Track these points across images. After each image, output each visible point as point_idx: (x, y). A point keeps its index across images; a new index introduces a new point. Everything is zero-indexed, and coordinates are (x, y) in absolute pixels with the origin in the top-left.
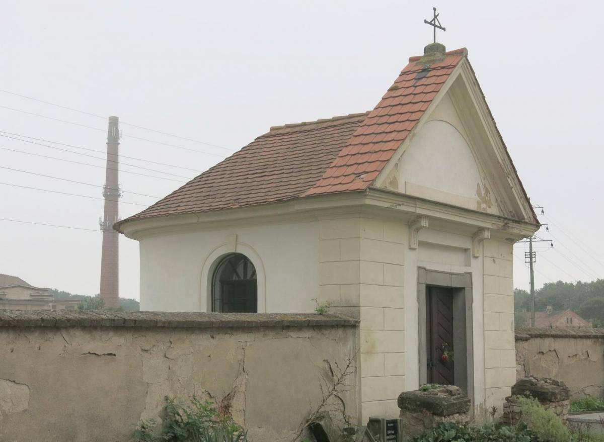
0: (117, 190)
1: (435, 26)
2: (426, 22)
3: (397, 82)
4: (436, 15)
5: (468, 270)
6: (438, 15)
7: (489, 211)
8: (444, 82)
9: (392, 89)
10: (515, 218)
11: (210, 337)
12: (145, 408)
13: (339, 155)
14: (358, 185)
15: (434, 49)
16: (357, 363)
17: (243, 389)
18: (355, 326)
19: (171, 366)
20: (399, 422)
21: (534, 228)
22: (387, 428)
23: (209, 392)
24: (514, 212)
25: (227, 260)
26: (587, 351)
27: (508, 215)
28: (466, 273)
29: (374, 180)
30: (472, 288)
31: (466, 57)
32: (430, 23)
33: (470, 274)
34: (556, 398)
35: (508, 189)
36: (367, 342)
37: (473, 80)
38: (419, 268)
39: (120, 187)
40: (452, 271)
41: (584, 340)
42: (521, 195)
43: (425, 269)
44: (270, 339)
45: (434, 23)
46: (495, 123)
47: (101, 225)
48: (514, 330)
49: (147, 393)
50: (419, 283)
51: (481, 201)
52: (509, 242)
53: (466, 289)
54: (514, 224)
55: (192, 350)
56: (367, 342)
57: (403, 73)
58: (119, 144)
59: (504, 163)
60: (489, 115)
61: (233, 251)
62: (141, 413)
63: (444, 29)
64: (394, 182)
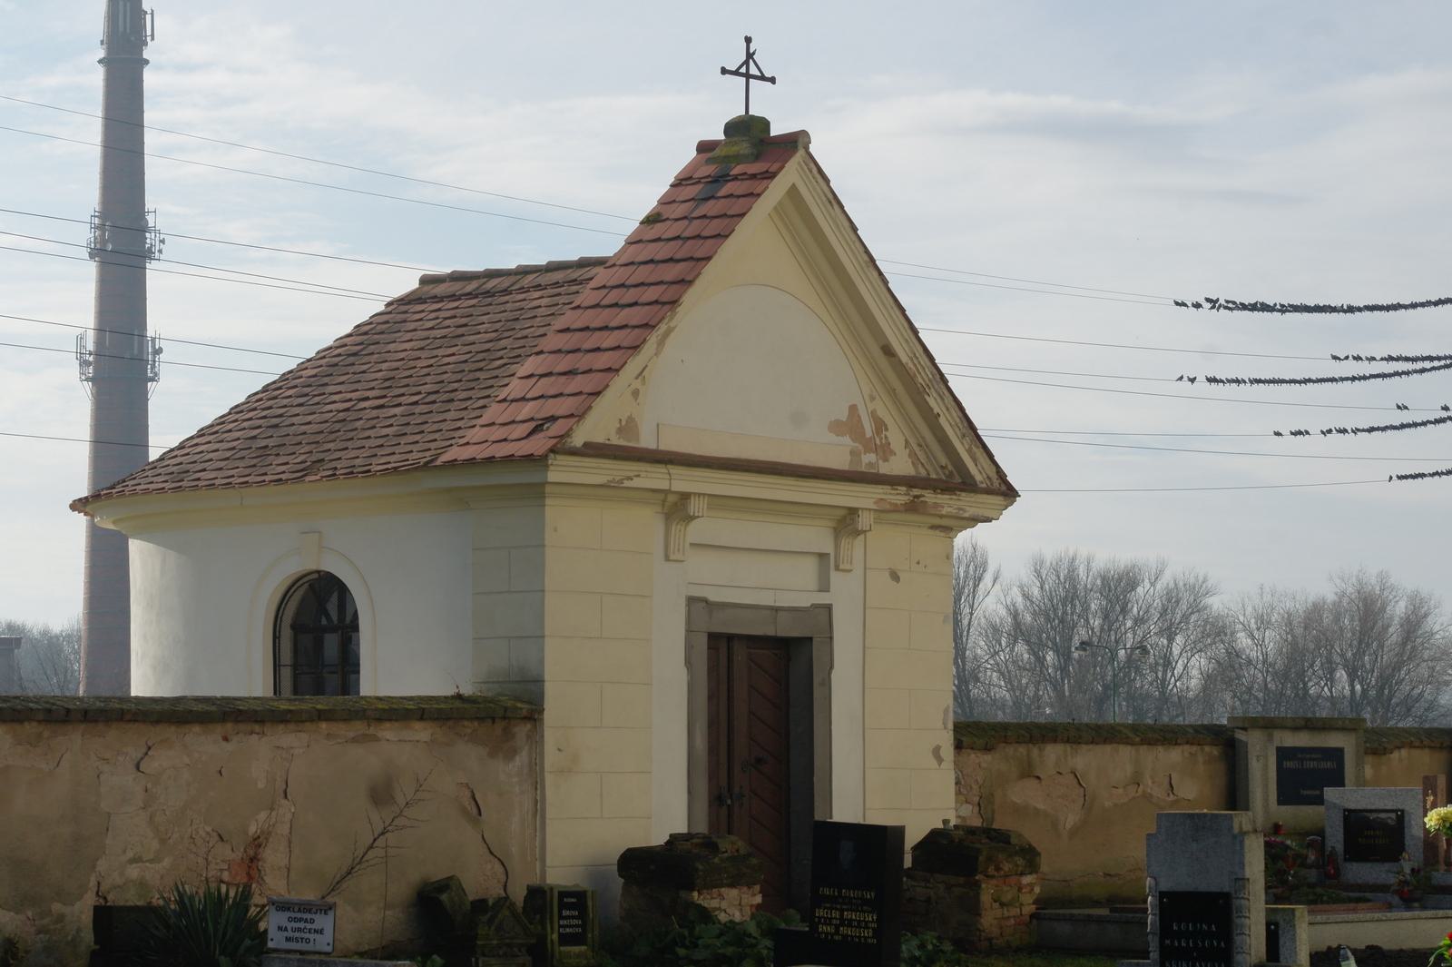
0: (142, 229)
1: (748, 76)
2: (724, 71)
3: (665, 204)
4: (751, 51)
5: (823, 599)
6: (754, 53)
7: (885, 469)
8: (743, 215)
9: (651, 220)
10: (960, 477)
11: (220, 738)
12: (104, 853)
13: (518, 375)
14: (538, 445)
15: (748, 129)
16: (538, 792)
17: (285, 829)
18: (534, 715)
19: (149, 786)
20: (589, 894)
21: (998, 500)
22: (559, 904)
23: (220, 832)
24: (950, 467)
25: (307, 582)
26: (1170, 775)
27: (937, 474)
28: (815, 606)
29: (568, 434)
30: (831, 638)
31: (807, 149)
32: (736, 73)
33: (829, 608)
34: (998, 869)
35: (931, 419)
36: (559, 750)
37: (826, 196)
38: (691, 600)
39: (151, 224)
40: (777, 604)
41: (1160, 748)
42: (964, 431)
43: (705, 601)
44: (340, 743)
45: (747, 71)
46: (885, 282)
47: (84, 364)
48: (951, 726)
49: (108, 830)
50: (689, 631)
51: (861, 447)
52: (942, 534)
53: (814, 640)
54: (939, 496)
55: (186, 760)
56: (559, 750)
57: (679, 183)
58: (147, 62)
59: (915, 365)
60: (870, 264)
61: (314, 567)
62: (97, 860)
63: (773, 80)
64: (628, 427)
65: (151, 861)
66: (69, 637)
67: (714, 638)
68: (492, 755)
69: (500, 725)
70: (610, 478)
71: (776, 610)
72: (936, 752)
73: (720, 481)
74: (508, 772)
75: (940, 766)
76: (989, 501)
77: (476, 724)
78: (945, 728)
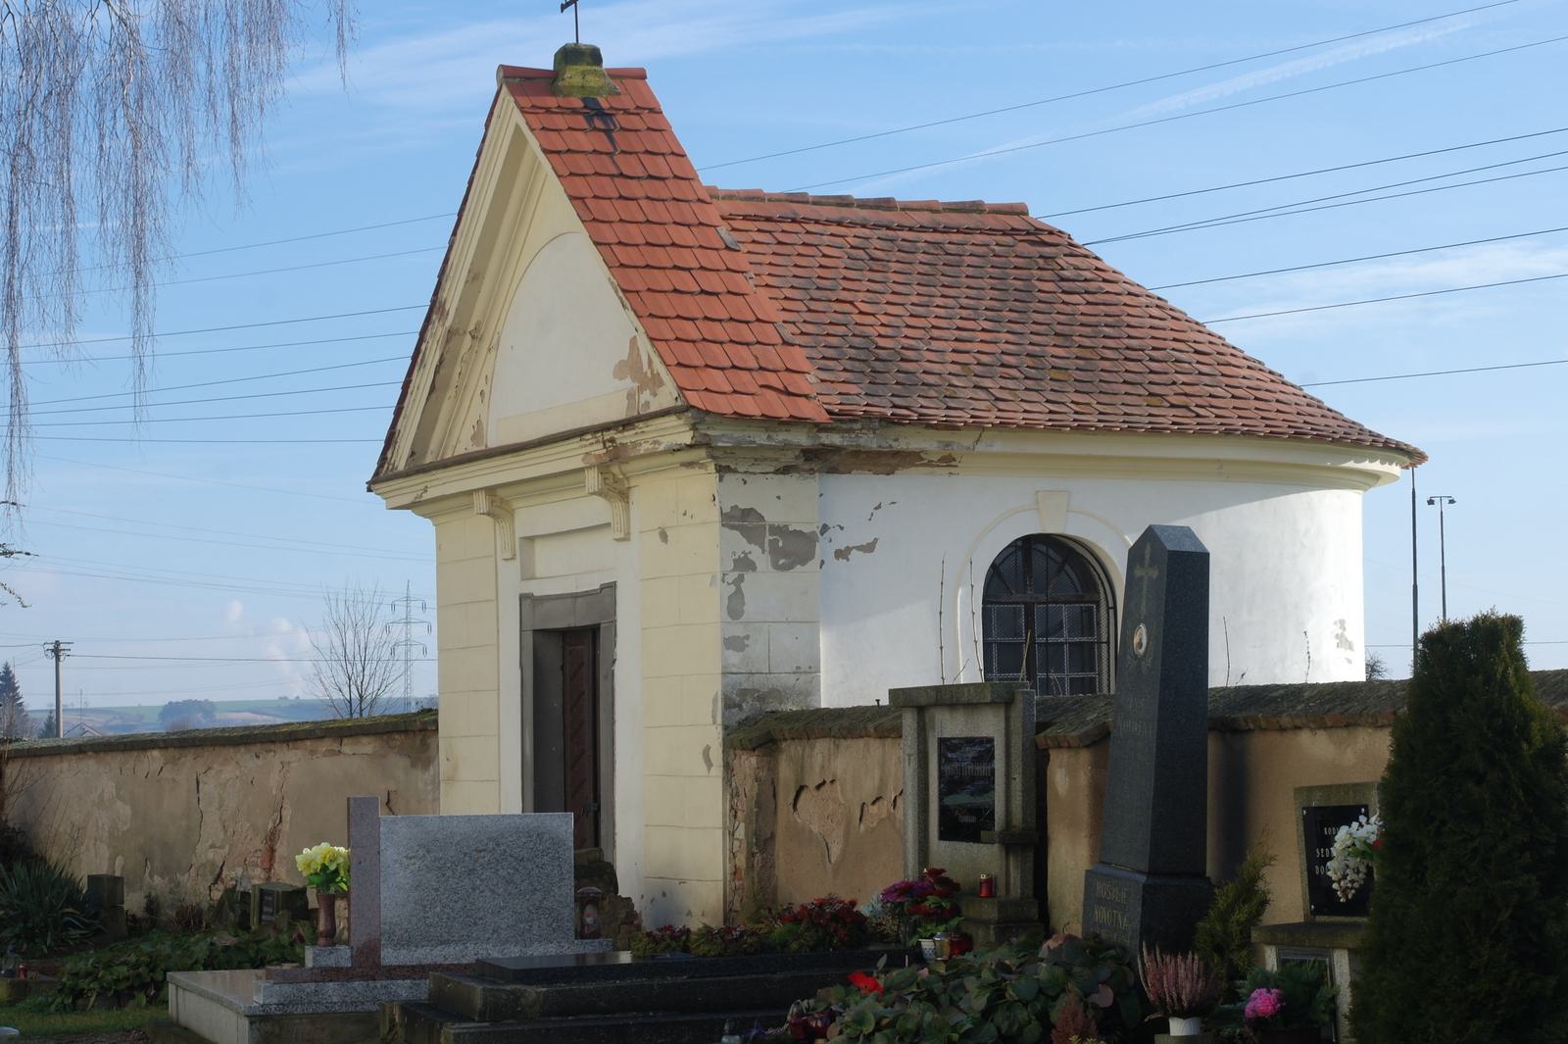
65: (220, 847)
66: (37, 716)
67: (541, 634)
68: (413, 765)
69: (419, 738)
70: (415, 494)
71: (575, 596)
72: (706, 751)
73: (505, 467)
74: (421, 778)
75: (709, 770)
76: (404, 485)
77: (403, 737)
78: (714, 723)
